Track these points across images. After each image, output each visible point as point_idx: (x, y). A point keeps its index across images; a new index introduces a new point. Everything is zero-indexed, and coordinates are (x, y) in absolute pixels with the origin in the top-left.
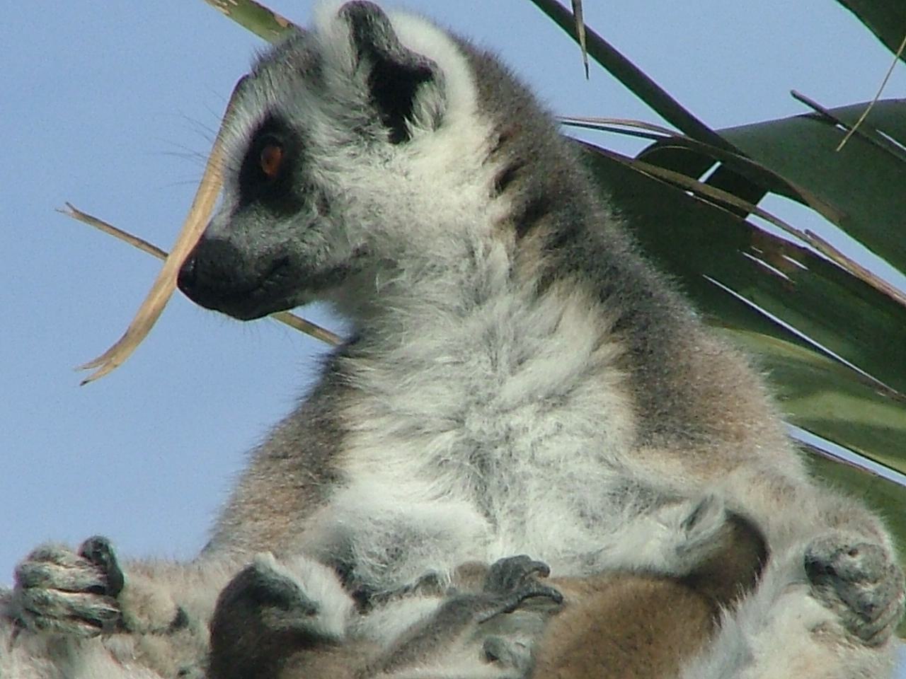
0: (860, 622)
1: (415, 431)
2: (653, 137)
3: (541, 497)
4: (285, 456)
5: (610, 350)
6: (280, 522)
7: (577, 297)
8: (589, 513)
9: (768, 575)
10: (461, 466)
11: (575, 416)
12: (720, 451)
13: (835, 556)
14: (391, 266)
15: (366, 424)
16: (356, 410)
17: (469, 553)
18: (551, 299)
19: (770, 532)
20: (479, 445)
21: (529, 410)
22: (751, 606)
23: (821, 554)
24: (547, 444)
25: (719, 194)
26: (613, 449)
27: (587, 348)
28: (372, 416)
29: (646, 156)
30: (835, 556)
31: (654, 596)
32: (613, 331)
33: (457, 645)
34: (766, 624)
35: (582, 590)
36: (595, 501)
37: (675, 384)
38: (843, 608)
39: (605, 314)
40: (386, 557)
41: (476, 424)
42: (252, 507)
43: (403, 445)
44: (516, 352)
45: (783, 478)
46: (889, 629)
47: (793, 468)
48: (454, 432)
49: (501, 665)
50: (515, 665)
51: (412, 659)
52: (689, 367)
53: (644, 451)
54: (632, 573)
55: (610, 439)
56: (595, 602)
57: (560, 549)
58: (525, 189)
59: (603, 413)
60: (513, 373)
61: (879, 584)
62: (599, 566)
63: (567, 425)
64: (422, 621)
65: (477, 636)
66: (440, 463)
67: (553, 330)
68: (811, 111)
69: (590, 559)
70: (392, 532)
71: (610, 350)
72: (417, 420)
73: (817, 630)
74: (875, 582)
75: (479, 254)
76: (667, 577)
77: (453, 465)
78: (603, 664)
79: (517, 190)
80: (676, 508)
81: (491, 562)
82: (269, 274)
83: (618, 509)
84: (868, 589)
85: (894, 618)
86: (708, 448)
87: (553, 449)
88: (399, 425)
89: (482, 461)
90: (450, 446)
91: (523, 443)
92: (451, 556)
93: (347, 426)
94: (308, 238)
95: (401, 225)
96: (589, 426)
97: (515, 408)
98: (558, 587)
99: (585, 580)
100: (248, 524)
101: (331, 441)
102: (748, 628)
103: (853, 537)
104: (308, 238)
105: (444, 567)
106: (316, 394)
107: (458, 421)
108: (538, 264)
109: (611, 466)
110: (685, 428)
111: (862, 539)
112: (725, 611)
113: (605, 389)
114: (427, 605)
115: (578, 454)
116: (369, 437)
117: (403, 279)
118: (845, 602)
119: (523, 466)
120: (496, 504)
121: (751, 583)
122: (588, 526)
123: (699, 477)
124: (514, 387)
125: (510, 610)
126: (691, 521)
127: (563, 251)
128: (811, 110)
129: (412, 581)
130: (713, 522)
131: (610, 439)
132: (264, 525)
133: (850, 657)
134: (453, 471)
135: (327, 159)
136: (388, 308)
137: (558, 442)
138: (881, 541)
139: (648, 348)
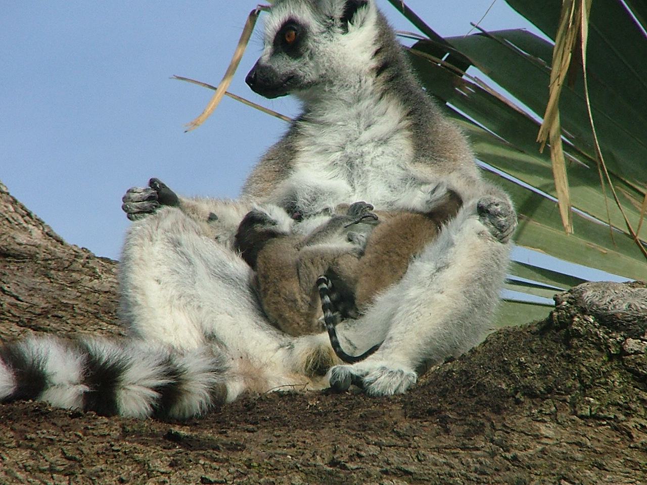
0: (498, 232)
1: (325, 151)
2: (417, 39)
3: (374, 179)
4: (272, 159)
5: (406, 123)
6: (267, 185)
7: (394, 101)
8: (392, 186)
9: (461, 211)
10: (342, 166)
11: (390, 148)
12: (447, 165)
13: (490, 205)
14: (331, 83)
15: (306, 148)
16: (302, 142)
17: (343, 200)
18: (383, 101)
19: (464, 196)
20: (350, 158)
21: (371, 145)
22: (453, 224)
23: (484, 204)
24: (378, 159)
25: (448, 65)
26: (404, 162)
27: (397, 121)
28: (308, 146)
29: (415, 46)
30: (490, 205)
31: (415, 218)
32: (408, 115)
33: (336, 235)
34: (459, 230)
35: (387, 217)
36: (395, 181)
37: (431, 138)
38: (492, 226)
39: (405, 109)
40: (310, 200)
41: (349, 150)
42: (257, 178)
43: (320, 156)
44: (368, 121)
45: (471, 177)
46: (509, 236)
47: (476, 174)
48: (341, 152)
49: (354, 243)
50: (359, 244)
51: (318, 240)
52: (436, 131)
53: (416, 164)
54: (407, 210)
55: (403, 158)
56: (391, 221)
57: (379, 199)
58: (383, 57)
59: (401, 148)
60: (365, 130)
61: (506, 218)
62: (394, 207)
63: (387, 152)
64: (322, 225)
65: (344, 232)
66: (334, 164)
67: (384, 114)
68: (480, 32)
69: (391, 204)
70: (313, 190)
71: (406, 123)
72: (326, 147)
73: (480, 234)
74: (505, 217)
75: (363, 82)
76: (421, 213)
77: (339, 165)
78: (394, 244)
79: (382, 57)
80: (427, 186)
81: (351, 204)
82: (285, 82)
83: (403, 185)
84: (502, 219)
85: (511, 232)
86: (441, 163)
87: (380, 161)
88: (319, 149)
89: (351, 165)
90: (339, 157)
91: (368, 158)
92: (336, 201)
93: (297, 149)
94: (302, 69)
95: (339, 66)
96: (395, 153)
97: (365, 144)
98: (377, 214)
99: (388, 212)
100: (254, 185)
101: (291, 154)
102: (452, 232)
103: (497, 199)
104: (302, 69)
105: (332, 205)
106: (288, 135)
107: (342, 148)
108: (381, 87)
109: (403, 169)
110: (433, 155)
111: (501, 200)
112: (444, 225)
113: (402, 138)
114: (325, 219)
115: (390, 164)
116: (306, 153)
117: (335, 89)
118: (493, 224)
119: (367, 167)
120: (356, 181)
121: (454, 215)
122: (392, 191)
123: (438, 175)
124: (366, 135)
125: (357, 223)
126: (433, 191)
127: (391, 84)
128: (480, 32)
129: (320, 210)
130: (442, 192)
131: (403, 158)
132: (261, 186)
133: (492, 245)
134: (339, 168)
135: (315, 38)
136: (323, 100)
137: (382, 158)
138: (552, 188)
139: (421, 123)
